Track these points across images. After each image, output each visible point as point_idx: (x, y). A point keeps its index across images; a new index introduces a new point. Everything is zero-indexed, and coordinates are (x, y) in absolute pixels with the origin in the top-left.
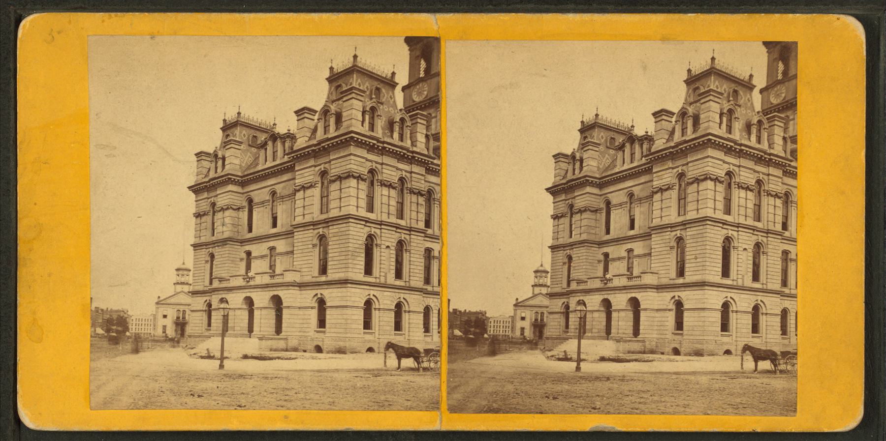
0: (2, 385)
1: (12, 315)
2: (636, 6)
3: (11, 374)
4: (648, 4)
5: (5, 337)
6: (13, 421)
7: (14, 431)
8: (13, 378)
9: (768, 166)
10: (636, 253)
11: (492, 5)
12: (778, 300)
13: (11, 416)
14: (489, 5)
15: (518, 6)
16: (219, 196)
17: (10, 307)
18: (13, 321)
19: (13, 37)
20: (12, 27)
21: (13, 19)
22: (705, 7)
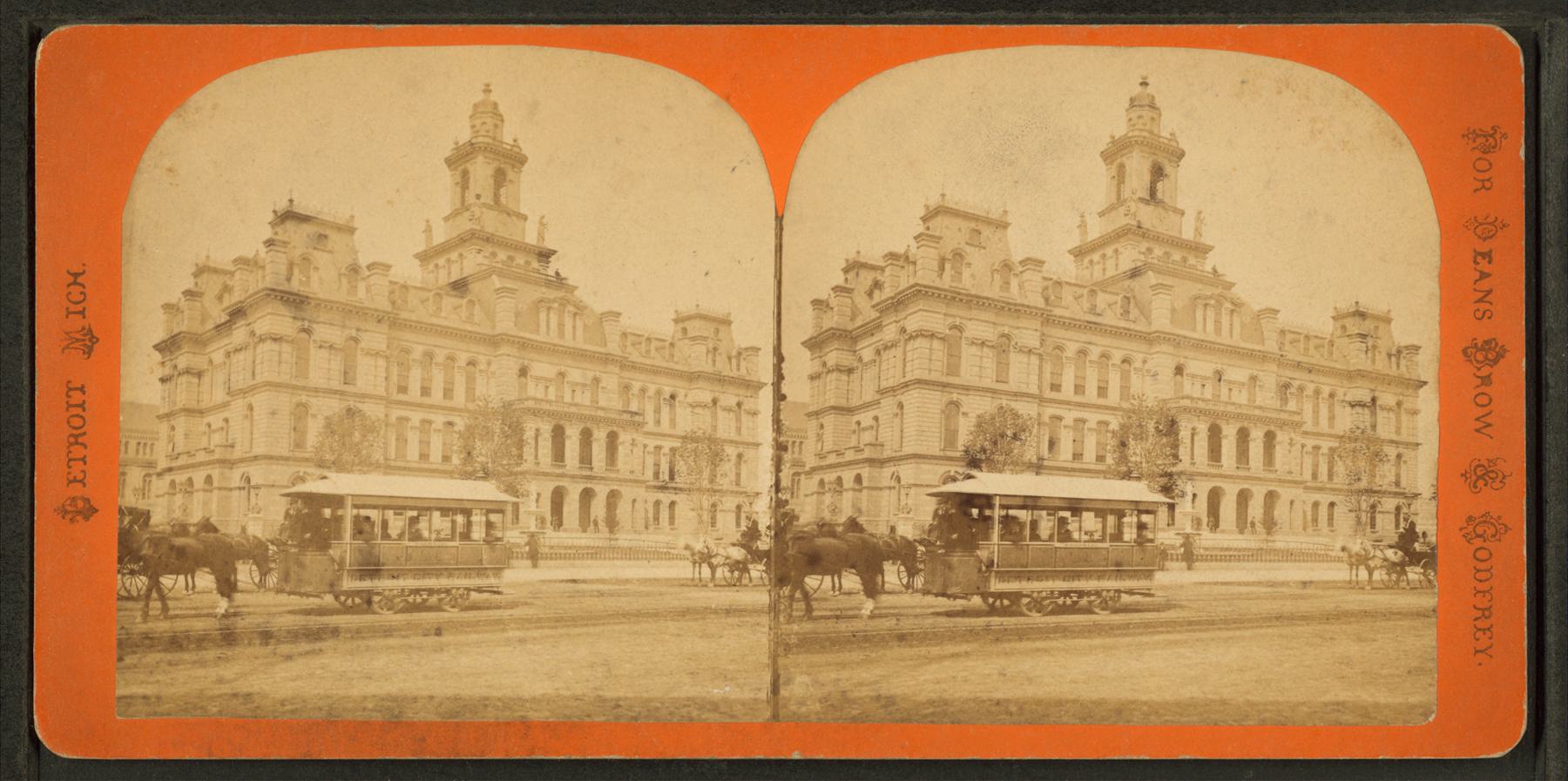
0: (3, 309)
1: (26, 553)
2: (1112, 12)
3: (24, 657)
4: (1134, 10)
5: (14, 592)
6: (27, 738)
7: (29, 756)
8: (26, 665)
9: (970, 308)
10: (863, 425)
11: (861, 11)
12: (914, 465)
13: (24, 732)
14: (855, 12)
15: (906, 14)
16: (973, 322)
17: (22, 540)
18: (26, 564)
19: (26, 69)
20: (26, 50)
21: (25, 32)
22: (1232, 15)
